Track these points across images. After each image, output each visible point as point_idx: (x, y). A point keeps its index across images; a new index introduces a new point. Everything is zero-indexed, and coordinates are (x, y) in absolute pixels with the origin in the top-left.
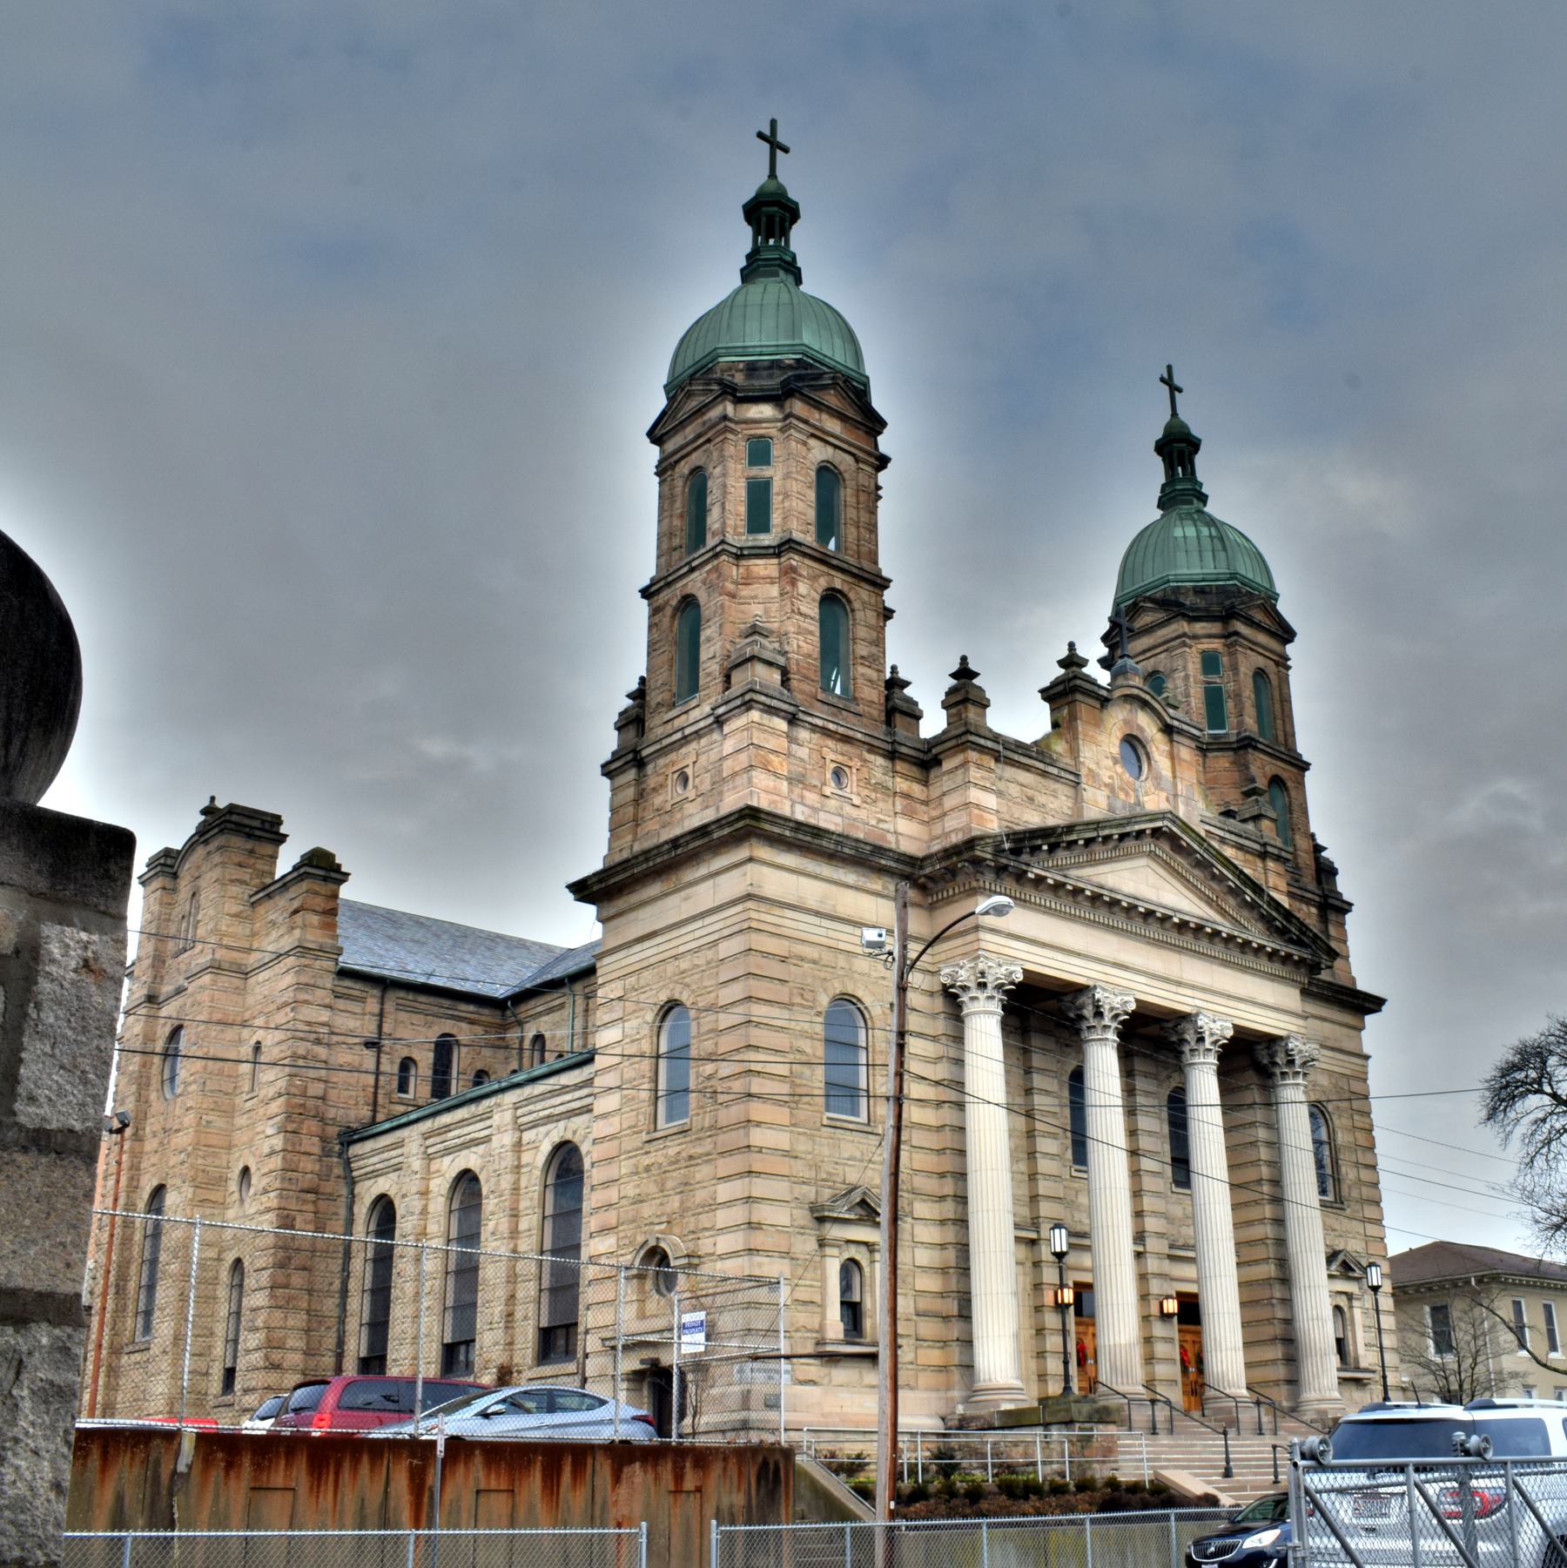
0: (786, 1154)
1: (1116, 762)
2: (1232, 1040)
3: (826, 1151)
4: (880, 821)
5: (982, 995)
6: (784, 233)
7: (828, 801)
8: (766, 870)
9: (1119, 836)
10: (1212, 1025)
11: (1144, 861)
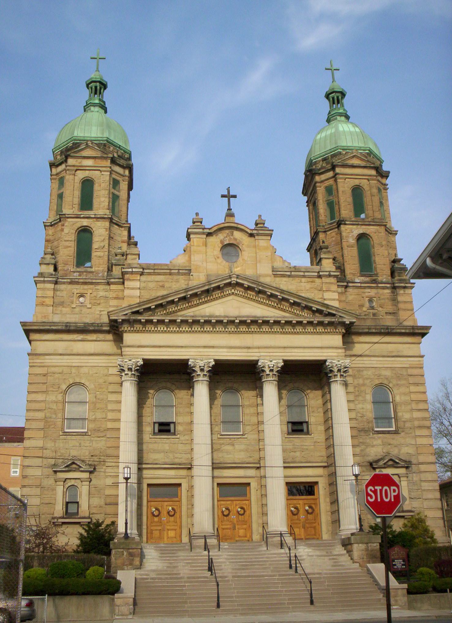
0: (42, 448)
2: (282, 367)
3: (61, 445)
4: (101, 311)
5: (202, 374)
8: (38, 343)
9: (209, 292)
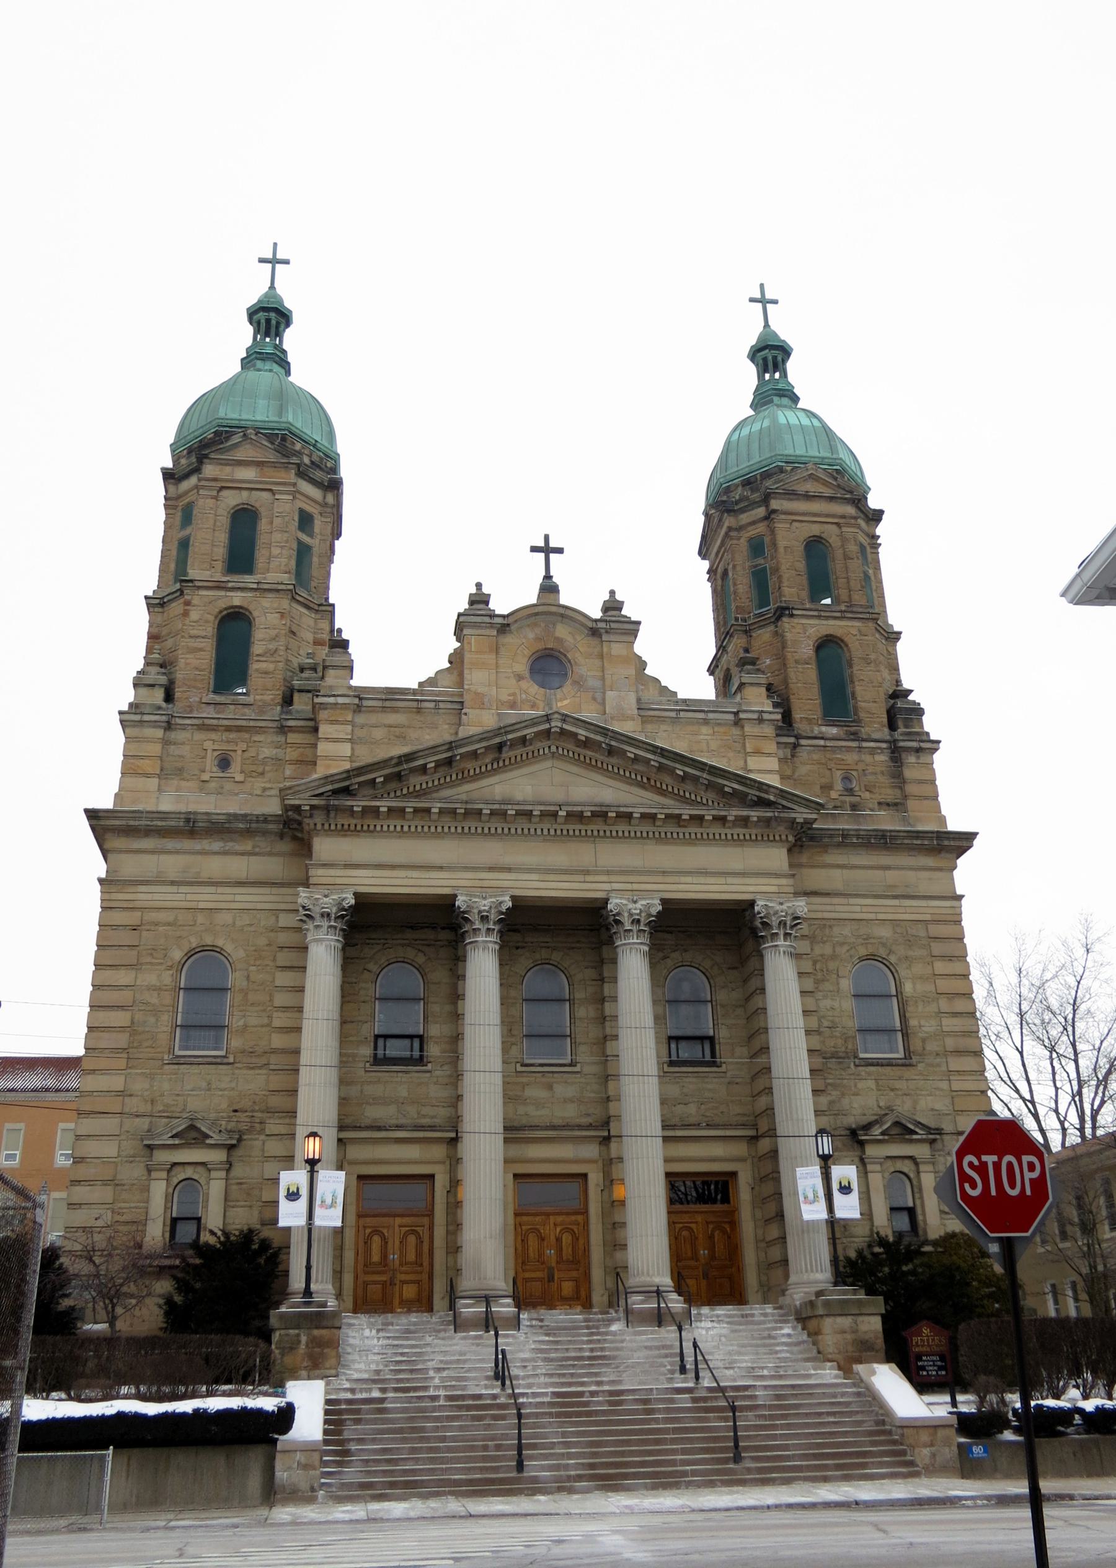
1: (520, 678)
3: (166, 1086)
6: (279, 334)
7: (207, 785)
8: (123, 856)
10: (631, 906)
11: (548, 763)
